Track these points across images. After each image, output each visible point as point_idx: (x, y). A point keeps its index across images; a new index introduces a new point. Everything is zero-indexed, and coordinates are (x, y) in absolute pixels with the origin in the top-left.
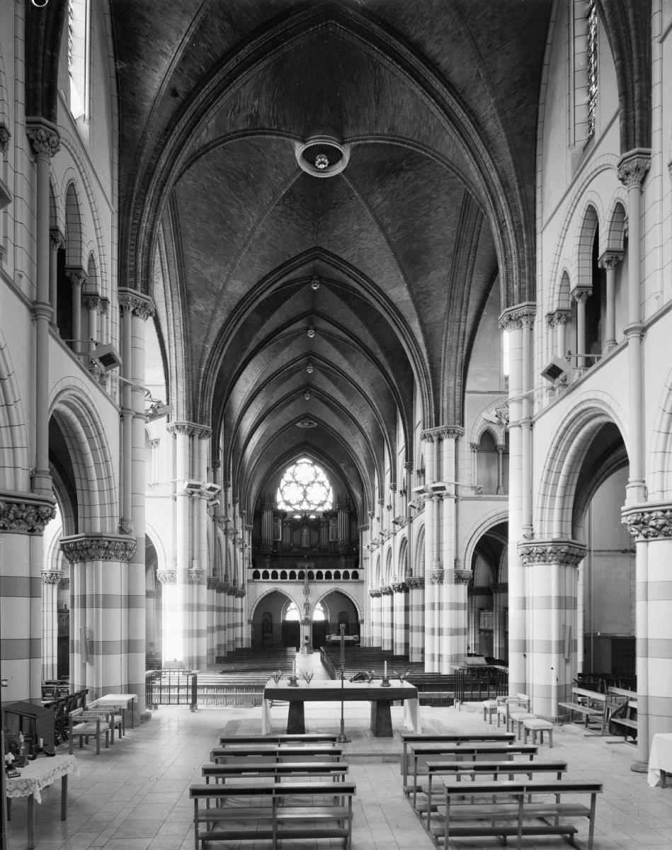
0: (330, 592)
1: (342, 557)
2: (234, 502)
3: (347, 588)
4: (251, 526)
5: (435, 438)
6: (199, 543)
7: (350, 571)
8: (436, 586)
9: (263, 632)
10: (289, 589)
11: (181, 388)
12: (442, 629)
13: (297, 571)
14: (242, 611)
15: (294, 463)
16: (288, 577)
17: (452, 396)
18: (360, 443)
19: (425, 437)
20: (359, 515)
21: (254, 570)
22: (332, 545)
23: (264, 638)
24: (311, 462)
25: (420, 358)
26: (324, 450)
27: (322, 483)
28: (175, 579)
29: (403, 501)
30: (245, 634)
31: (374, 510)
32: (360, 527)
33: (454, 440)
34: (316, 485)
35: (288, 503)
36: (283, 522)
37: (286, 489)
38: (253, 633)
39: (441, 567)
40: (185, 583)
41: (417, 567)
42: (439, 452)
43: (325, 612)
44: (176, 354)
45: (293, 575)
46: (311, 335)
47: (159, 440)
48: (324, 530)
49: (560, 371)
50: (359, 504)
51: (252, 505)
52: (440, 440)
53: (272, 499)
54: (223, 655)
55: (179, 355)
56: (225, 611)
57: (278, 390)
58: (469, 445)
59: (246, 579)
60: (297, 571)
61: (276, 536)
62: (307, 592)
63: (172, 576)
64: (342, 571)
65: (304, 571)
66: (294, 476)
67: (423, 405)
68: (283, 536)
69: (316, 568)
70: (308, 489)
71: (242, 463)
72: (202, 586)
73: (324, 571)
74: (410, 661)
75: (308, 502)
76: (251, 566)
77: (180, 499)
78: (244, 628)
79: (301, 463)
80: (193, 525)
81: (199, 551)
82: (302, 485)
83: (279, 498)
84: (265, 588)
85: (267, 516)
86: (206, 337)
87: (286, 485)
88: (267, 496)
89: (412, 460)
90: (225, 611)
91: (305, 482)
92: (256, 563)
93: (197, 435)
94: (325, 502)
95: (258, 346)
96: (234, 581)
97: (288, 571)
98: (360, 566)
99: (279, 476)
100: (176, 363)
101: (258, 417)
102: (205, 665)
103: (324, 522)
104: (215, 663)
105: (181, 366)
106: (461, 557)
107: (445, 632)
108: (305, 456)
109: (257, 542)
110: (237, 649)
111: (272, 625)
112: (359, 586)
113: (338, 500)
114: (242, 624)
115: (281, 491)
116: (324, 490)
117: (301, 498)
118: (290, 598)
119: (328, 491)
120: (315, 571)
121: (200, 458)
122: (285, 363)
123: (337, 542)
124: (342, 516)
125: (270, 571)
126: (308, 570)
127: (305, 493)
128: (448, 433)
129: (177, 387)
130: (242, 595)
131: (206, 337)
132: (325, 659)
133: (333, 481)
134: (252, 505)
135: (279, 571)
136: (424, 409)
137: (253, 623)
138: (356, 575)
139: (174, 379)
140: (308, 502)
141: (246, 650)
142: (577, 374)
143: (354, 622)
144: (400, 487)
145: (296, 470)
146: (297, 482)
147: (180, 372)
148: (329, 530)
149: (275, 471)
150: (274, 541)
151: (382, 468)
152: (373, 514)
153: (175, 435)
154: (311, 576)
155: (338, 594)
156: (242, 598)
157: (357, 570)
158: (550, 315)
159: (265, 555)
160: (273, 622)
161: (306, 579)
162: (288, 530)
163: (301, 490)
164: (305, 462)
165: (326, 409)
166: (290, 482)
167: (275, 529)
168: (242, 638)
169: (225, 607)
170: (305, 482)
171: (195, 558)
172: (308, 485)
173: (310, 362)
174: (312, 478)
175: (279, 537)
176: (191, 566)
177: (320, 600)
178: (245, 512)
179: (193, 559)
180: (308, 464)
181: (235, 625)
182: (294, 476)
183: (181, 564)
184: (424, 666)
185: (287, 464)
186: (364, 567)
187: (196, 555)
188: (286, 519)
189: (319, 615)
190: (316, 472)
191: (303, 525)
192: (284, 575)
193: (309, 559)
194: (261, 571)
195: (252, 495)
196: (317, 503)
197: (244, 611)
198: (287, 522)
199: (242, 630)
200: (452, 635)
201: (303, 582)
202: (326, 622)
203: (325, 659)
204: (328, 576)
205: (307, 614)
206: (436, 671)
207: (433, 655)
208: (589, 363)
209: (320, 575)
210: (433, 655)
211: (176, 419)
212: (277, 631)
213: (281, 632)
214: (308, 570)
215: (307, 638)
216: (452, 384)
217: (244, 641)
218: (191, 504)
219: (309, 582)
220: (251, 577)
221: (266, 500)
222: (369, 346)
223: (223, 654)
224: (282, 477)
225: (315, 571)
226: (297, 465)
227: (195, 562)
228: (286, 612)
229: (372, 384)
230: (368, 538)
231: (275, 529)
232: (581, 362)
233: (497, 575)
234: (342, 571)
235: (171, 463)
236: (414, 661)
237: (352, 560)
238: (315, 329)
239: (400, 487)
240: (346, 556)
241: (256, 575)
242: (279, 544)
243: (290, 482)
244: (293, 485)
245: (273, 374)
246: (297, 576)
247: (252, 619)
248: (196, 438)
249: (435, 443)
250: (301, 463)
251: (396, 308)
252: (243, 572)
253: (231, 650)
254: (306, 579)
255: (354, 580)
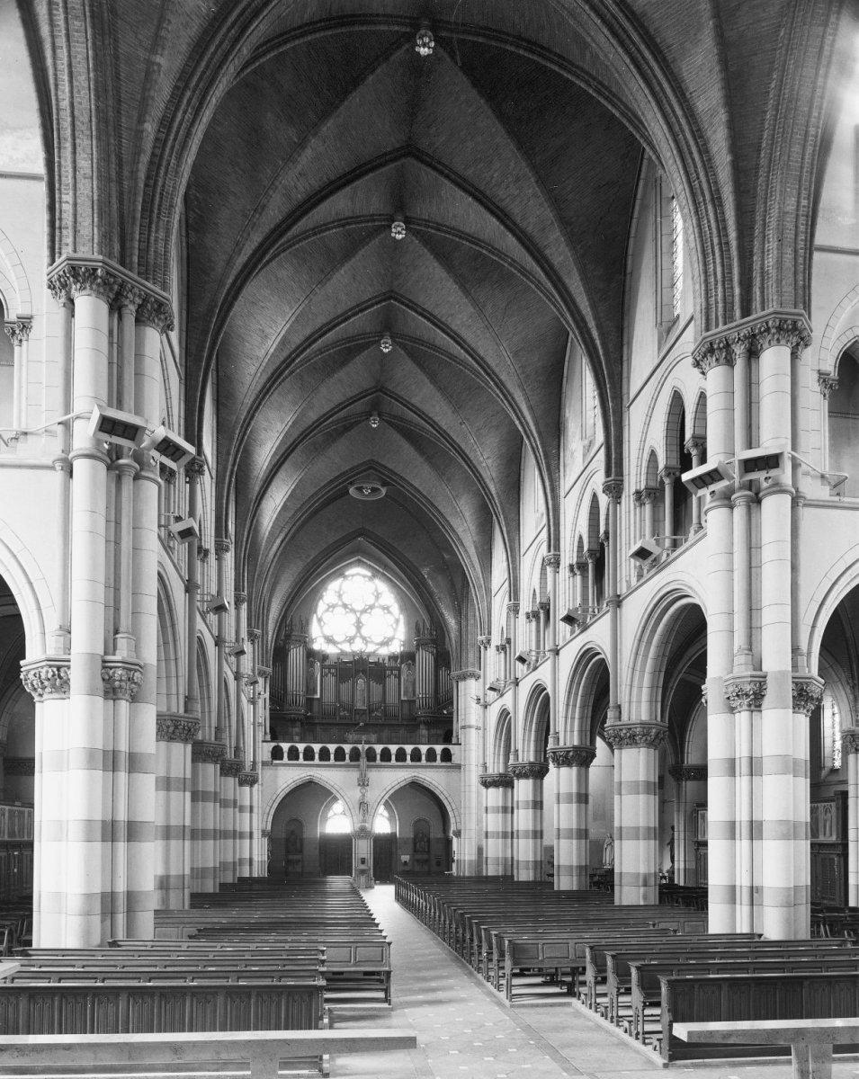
0: (402, 784)
1: (421, 727)
2: (238, 602)
3: (433, 777)
4: (270, 670)
5: (739, 350)
6: (136, 594)
7: (439, 748)
8: (743, 717)
9: (288, 852)
10: (330, 776)
11: (84, 164)
12: (761, 823)
13: (347, 748)
14: (251, 811)
15: (340, 574)
16: (332, 756)
17: (790, 235)
18: (467, 514)
19: (711, 351)
20: (453, 655)
21: (273, 744)
22: (406, 705)
23: (289, 862)
24: (369, 574)
25: (700, 152)
26: (395, 545)
27: (386, 609)
28: (66, 683)
29: (500, 661)
30: (255, 855)
31: (490, 633)
32: (454, 673)
33: (788, 351)
34: (377, 611)
35: (329, 640)
36: (323, 667)
37: (326, 617)
38: (272, 852)
39: (758, 665)
40: (92, 693)
41: (634, 699)
42: (751, 384)
43: (391, 819)
44: (70, 65)
45: (340, 755)
46: (398, 232)
47: (30, 318)
48: (391, 682)
49: (650, 553)
50: (453, 635)
51: (270, 634)
52: (753, 354)
53: (305, 626)
54: (211, 891)
55: (80, 68)
56: (234, 838)
57: (323, 390)
58: (816, 376)
59: (259, 759)
60: (347, 748)
61: (310, 689)
62: (363, 783)
63: (59, 681)
64: (424, 749)
65: (360, 746)
66: (340, 596)
67: (706, 272)
68: (325, 689)
69: (379, 742)
70: (364, 618)
71: (255, 529)
72: (142, 705)
73: (393, 748)
74: (617, 902)
75: (364, 639)
76: (268, 737)
77: (81, 467)
78: (255, 841)
79: (353, 576)
80: (117, 543)
81: (136, 613)
82: (353, 611)
83: (315, 630)
84: (288, 776)
85: (296, 656)
86: (157, 35)
87: (327, 610)
88: (296, 621)
89: (620, 473)
90: (234, 838)
91: (359, 606)
92: (277, 731)
93: (132, 308)
94: (391, 639)
95: (289, 216)
96: (237, 749)
97: (332, 748)
98: (454, 740)
99: (316, 594)
100: (72, 92)
101: (282, 442)
102: (151, 914)
103: (392, 669)
104: (187, 907)
105: (86, 101)
106: (804, 646)
107: (767, 765)
108: (359, 563)
109: (278, 698)
110: (241, 879)
111: (302, 840)
112: (454, 774)
113: (416, 629)
114: (251, 833)
115: (320, 620)
116: (391, 619)
117: (353, 631)
118: (334, 792)
119: (397, 621)
120: (378, 748)
121: (139, 374)
122: (340, 311)
123: (415, 701)
124: (425, 659)
125: (301, 747)
126: (367, 746)
127: (359, 625)
128: (780, 329)
129: (74, 162)
130: (251, 781)
131: (157, 35)
132: (414, 897)
133: (406, 606)
134: (270, 634)
135: (317, 747)
136: (706, 282)
137: (271, 836)
138: (447, 756)
139: (68, 145)
140: (364, 639)
141: (259, 880)
142: (665, 555)
143: (440, 835)
144: (526, 605)
145: (343, 587)
146: (345, 606)
147: (83, 117)
148: (400, 681)
149: (310, 584)
150: (307, 699)
151: (517, 545)
152: (489, 641)
153: (72, 301)
154: (371, 755)
155: (416, 787)
156: (251, 786)
157: (450, 747)
158: (527, 614)
159: (293, 721)
160: (305, 836)
161: (363, 761)
162: (331, 680)
163: (352, 618)
164: (358, 574)
165: (408, 449)
166: (334, 606)
167: (309, 679)
168: (251, 860)
169: (235, 831)
170: (359, 606)
171: (122, 629)
172: (364, 611)
173: (387, 326)
174: (371, 601)
175: (315, 692)
176: (111, 646)
177: (383, 801)
178: (258, 632)
179: (116, 632)
180: (364, 576)
181: (236, 835)
182: (340, 596)
183: (85, 642)
184: (703, 906)
185: (328, 577)
186: (462, 740)
187: (125, 622)
188: (327, 663)
189: (382, 824)
190: (376, 590)
191: (357, 672)
192: (324, 755)
193: (367, 728)
194: (285, 746)
195: (271, 616)
196: (379, 640)
197: (255, 810)
198: (329, 667)
199: (251, 817)
200: (786, 837)
201: (358, 766)
202: (393, 835)
203: (414, 897)
204: (401, 756)
205: (364, 821)
206: (742, 927)
207: (732, 889)
208: (675, 545)
209: (386, 755)
210: (732, 889)
211: (70, 249)
212: (311, 852)
213: (317, 852)
214: (367, 746)
215: (363, 861)
216: (791, 205)
217: (255, 865)
218: (113, 486)
219: (368, 767)
220: (267, 756)
221: (291, 630)
222: (530, 229)
223: (210, 887)
224: (321, 598)
225: (378, 748)
226: (345, 577)
227: (122, 642)
228: (325, 819)
229: (516, 354)
230: (469, 692)
231: (309, 679)
232: (667, 543)
233: (682, 753)
234: (424, 749)
235: (59, 380)
236: (625, 903)
237: (439, 732)
238: (407, 221)
239: (526, 605)
240: (429, 725)
241: (276, 753)
242: (315, 703)
243: (334, 606)
244: (340, 610)
245: (317, 331)
246: (347, 756)
247: (269, 828)
248: (129, 319)
249: (739, 364)
250: (353, 576)
251: (642, 26)
252: (256, 747)
253: (230, 880)
254: (363, 761)
255: (444, 764)
